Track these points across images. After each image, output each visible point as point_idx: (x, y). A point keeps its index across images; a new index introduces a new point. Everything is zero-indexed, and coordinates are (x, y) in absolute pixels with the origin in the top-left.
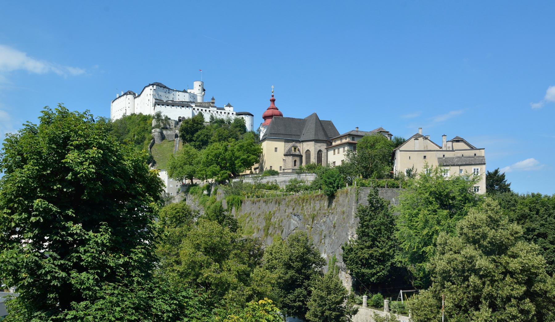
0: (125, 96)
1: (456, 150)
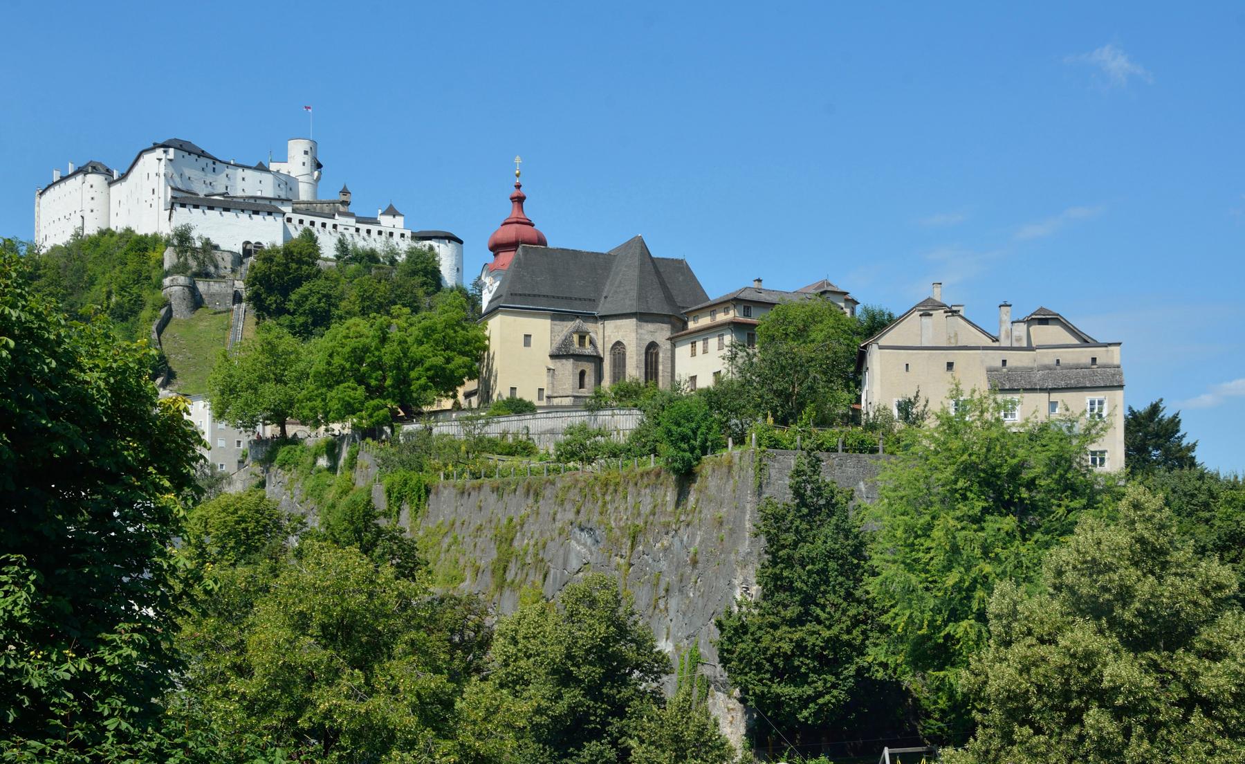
0: (80, 177)
1: (1039, 347)
